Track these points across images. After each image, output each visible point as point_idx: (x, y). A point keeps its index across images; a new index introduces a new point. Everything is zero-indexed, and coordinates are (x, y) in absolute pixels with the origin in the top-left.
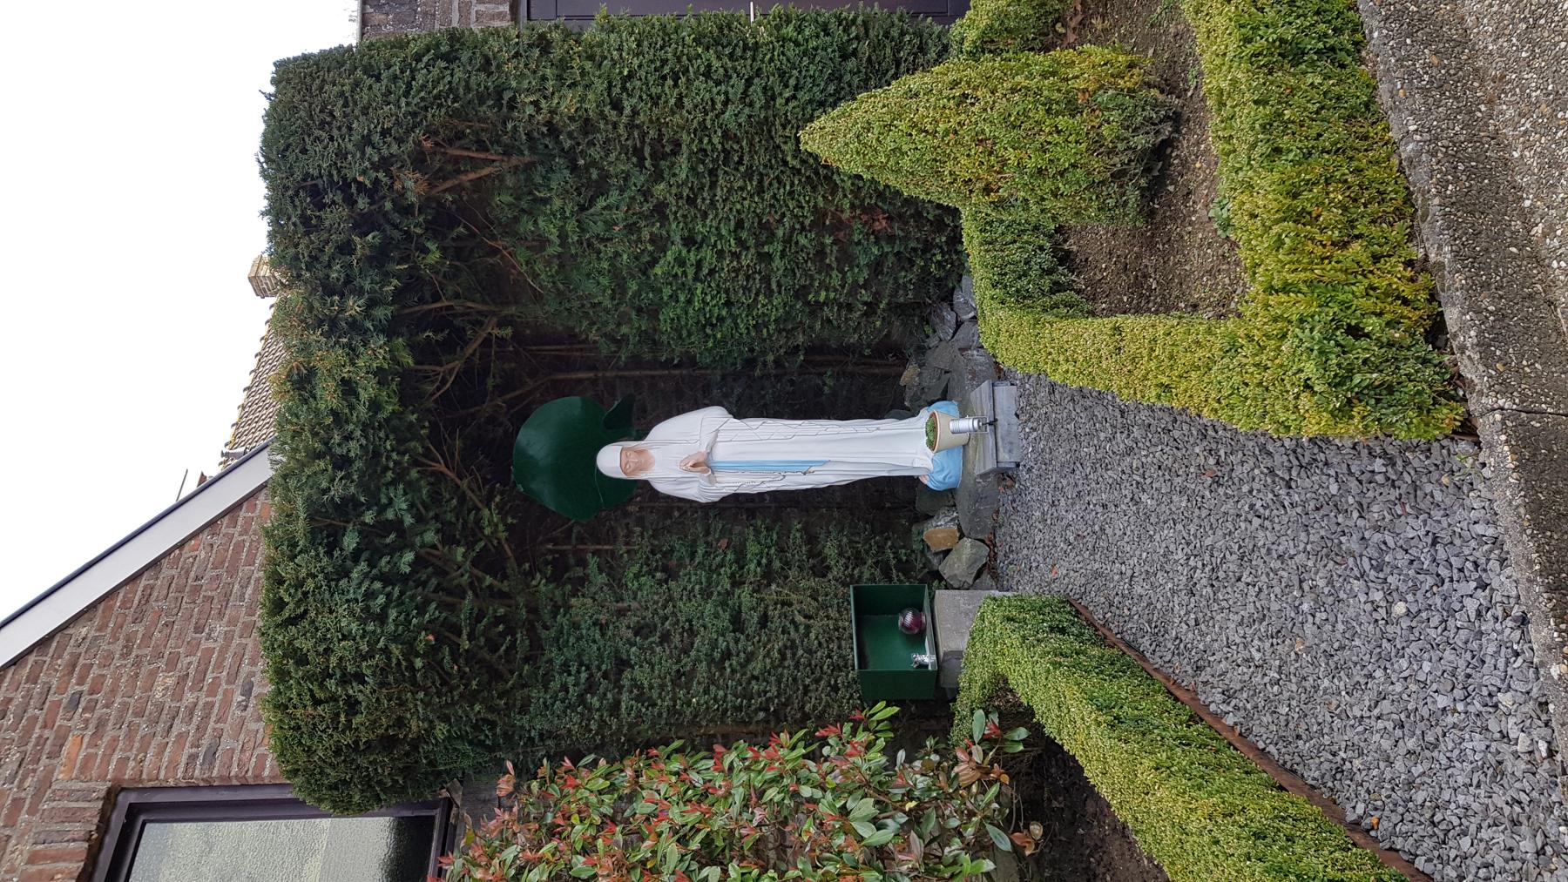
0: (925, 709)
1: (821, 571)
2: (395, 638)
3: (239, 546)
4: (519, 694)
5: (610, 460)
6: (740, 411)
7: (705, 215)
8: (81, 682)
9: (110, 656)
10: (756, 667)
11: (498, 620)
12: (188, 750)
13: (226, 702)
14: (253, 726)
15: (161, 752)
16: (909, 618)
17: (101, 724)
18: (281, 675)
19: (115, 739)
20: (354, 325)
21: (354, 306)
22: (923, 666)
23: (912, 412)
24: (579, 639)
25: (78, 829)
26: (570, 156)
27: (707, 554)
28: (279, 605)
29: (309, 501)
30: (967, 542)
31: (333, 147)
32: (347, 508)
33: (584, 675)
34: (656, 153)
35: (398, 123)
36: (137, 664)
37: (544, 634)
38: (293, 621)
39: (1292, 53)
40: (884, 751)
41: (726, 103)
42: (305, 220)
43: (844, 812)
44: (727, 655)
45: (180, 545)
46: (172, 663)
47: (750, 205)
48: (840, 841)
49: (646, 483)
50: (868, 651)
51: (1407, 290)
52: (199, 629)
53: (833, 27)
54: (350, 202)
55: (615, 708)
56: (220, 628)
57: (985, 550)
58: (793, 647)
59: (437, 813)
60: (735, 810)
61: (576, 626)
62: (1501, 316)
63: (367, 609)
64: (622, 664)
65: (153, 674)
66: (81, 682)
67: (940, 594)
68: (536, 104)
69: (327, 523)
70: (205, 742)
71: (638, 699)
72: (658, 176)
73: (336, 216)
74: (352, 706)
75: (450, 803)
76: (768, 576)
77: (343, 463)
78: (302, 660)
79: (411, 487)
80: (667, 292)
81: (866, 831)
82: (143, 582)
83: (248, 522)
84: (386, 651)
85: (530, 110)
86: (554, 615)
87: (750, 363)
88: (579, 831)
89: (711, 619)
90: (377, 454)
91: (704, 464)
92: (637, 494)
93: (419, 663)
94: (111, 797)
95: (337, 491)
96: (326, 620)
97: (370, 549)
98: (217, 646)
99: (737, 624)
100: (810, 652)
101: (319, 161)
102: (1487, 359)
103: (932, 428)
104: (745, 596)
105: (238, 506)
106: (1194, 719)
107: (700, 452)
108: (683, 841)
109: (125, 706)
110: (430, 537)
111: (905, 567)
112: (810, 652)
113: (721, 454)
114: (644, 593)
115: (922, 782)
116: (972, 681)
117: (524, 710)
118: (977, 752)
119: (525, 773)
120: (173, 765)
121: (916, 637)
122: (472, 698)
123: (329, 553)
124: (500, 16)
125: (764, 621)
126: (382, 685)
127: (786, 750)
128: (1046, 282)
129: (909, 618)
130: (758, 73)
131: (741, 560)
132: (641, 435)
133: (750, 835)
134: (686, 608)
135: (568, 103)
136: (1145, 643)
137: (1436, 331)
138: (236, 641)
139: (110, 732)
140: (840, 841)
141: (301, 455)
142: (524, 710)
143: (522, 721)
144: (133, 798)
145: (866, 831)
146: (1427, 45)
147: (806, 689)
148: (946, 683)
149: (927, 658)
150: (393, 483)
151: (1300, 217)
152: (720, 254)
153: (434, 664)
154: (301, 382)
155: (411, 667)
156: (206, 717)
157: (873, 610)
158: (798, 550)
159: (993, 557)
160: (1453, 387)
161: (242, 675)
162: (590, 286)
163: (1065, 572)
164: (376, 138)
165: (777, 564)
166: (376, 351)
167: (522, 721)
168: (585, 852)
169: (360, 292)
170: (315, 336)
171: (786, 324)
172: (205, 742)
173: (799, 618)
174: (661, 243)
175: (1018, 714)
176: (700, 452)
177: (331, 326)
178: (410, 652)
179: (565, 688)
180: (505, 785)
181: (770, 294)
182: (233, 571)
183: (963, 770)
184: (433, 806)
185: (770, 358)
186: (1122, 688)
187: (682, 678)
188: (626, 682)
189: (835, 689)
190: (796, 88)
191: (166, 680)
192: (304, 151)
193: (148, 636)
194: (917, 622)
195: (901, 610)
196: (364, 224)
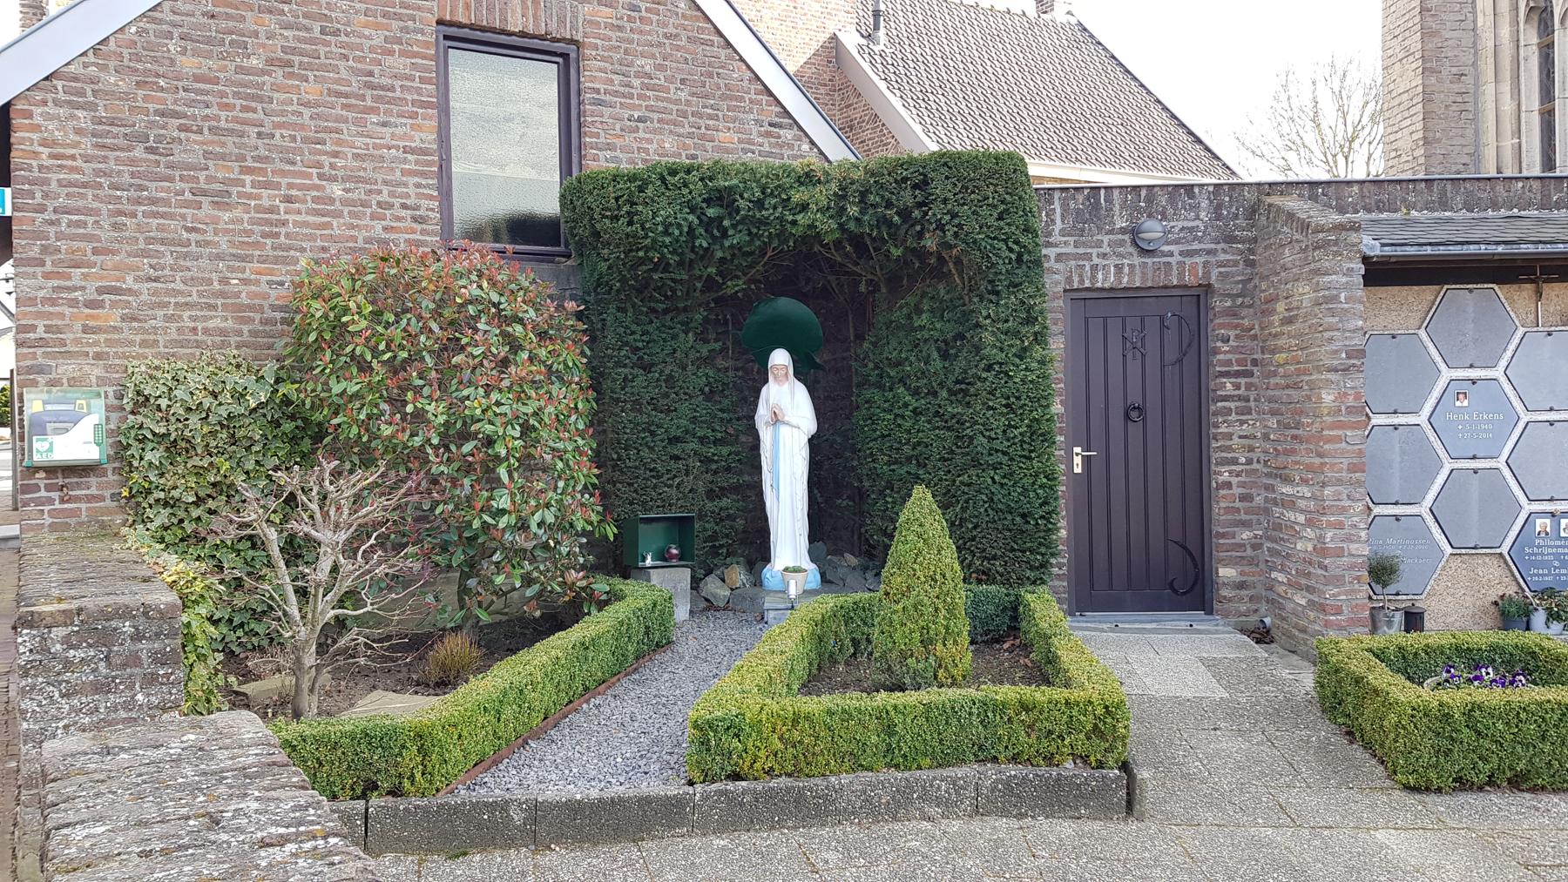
0: (617, 560)
1: (711, 495)
2: (654, 241)
3: (742, 99)
4: (628, 305)
5: (780, 358)
6: (814, 443)
7: (929, 422)
8: (647, 10)
9: (665, 25)
10: (645, 453)
11: (674, 291)
12: (602, 87)
13: (633, 107)
14: (618, 127)
15: (601, 70)
16: (675, 551)
17: (620, 28)
18: (632, 178)
19: (610, 39)
20: (843, 209)
21: (853, 210)
22: (644, 559)
23: (814, 557)
24: (665, 340)
25: (553, 26)
26: (961, 336)
27: (722, 419)
28: (673, 172)
29: (730, 189)
30: (728, 593)
31: (950, 195)
32: (732, 208)
33: (640, 345)
34: (962, 390)
35: (967, 234)
36: (660, 44)
37: (668, 317)
38: (663, 179)
39: (890, 730)
40: (584, 529)
41: (989, 438)
42: (905, 180)
43: (548, 506)
44: (653, 434)
45: (742, 60)
46: (660, 68)
47: (936, 450)
48: (533, 503)
49: (766, 381)
50: (654, 525)
51: (757, 765)
52: (683, 81)
53: (1046, 508)
54: (920, 205)
55: (618, 364)
56: (683, 95)
57: (722, 605)
58: (658, 477)
59: (562, 249)
60: (551, 443)
61: (674, 337)
62: (741, 804)
63: (671, 224)
64: (648, 368)
65: (653, 56)
66: (647, 10)
67: (686, 574)
68: (989, 316)
69: (725, 198)
70: (608, 98)
71: (625, 379)
72: (951, 392)
73: (907, 197)
74: (616, 218)
75: (568, 256)
76: (706, 461)
77: (760, 204)
78: (641, 190)
79: (750, 243)
80: (891, 395)
81: (537, 517)
82: (716, 39)
83: (759, 103)
84: (646, 236)
85: (984, 313)
86: (682, 323)
87: (855, 451)
88: (543, 353)
89: (678, 424)
90: (766, 224)
91: (776, 420)
92: (761, 377)
93: (641, 254)
94: (572, 41)
95: (742, 203)
96: (664, 201)
97: (708, 224)
98: (671, 95)
99: (674, 440)
100: (655, 487)
101: (939, 188)
102: (720, 793)
103: (797, 570)
104: (693, 445)
105: (770, 94)
106: (586, 689)
107: (787, 415)
108: (535, 414)
109: (631, 42)
110: (719, 254)
111: (714, 551)
112: (655, 487)
113: (783, 429)
114: (698, 379)
115: (564, 550)
116: (628, 586)
117: (619, 309)
118: (584, 583)
119: (579, 316)
120: (593, 79)
121: (663, 556)
122: (623, 280)
123: (704, 200)
124: (1082, 281)
125: (676, 458)
126: (627, 235)
127: (586, 472)
128: (858, 636)
129: (675, 551)
130: (1012, 459)
131: (716, 442)
132: (797, 375)
133: (536, 452)
134: (684, 408)
135: (988, 338)
136: (636, 676)
137: (736, 777)
138: (675, 108)
139: (614, 35)
140: (533, 503)
141: (764, 180)
142: (619, 309)
143: (612, 309)
144: (573, 55)
145: (537, 517)
146: (893, 798)
147: (630, 485)
148: (633, 572)
149: (649, 562)
150: (750, 233)
151: (795, 722)
152: (909, 432)
153: (642, 261)
154: (807, 178)
155: (638, 250)
156: (624, 96)
157: (681, 527)
158: (723, 480)
159: (717, 609)
160: (708, 778)
161: (651, 115)
162: (894, 343)
163: (688, 645)
164: (956, 221)
165: (714, 467)
166: (827, 225)
167: (612, 309)
168: (531, 359)
169: (863, 212)
170: (834, 187)
171: (874, 475)
172: (608, 98)
173: (677, 480)
174: (916, 393)
175: (602, 605)
176: (787, 415)
177: (842, 197)
178: (647, 249)
179: (633, 333)
180: (571, 305)
181: (889, 463)
182: (723, 97)
183: (573, 575)
184: (566, 246)
185: (855, 463)
186: (605, 655)
187: (637, 406)
188: (636, 371)
189: (631, 503)
190: (1002, 485)
191: (647, 65)
192: (947, 178)
193: (678, 48)
194: (672, 557)
195: (680, 547)
196: (905, 214)
